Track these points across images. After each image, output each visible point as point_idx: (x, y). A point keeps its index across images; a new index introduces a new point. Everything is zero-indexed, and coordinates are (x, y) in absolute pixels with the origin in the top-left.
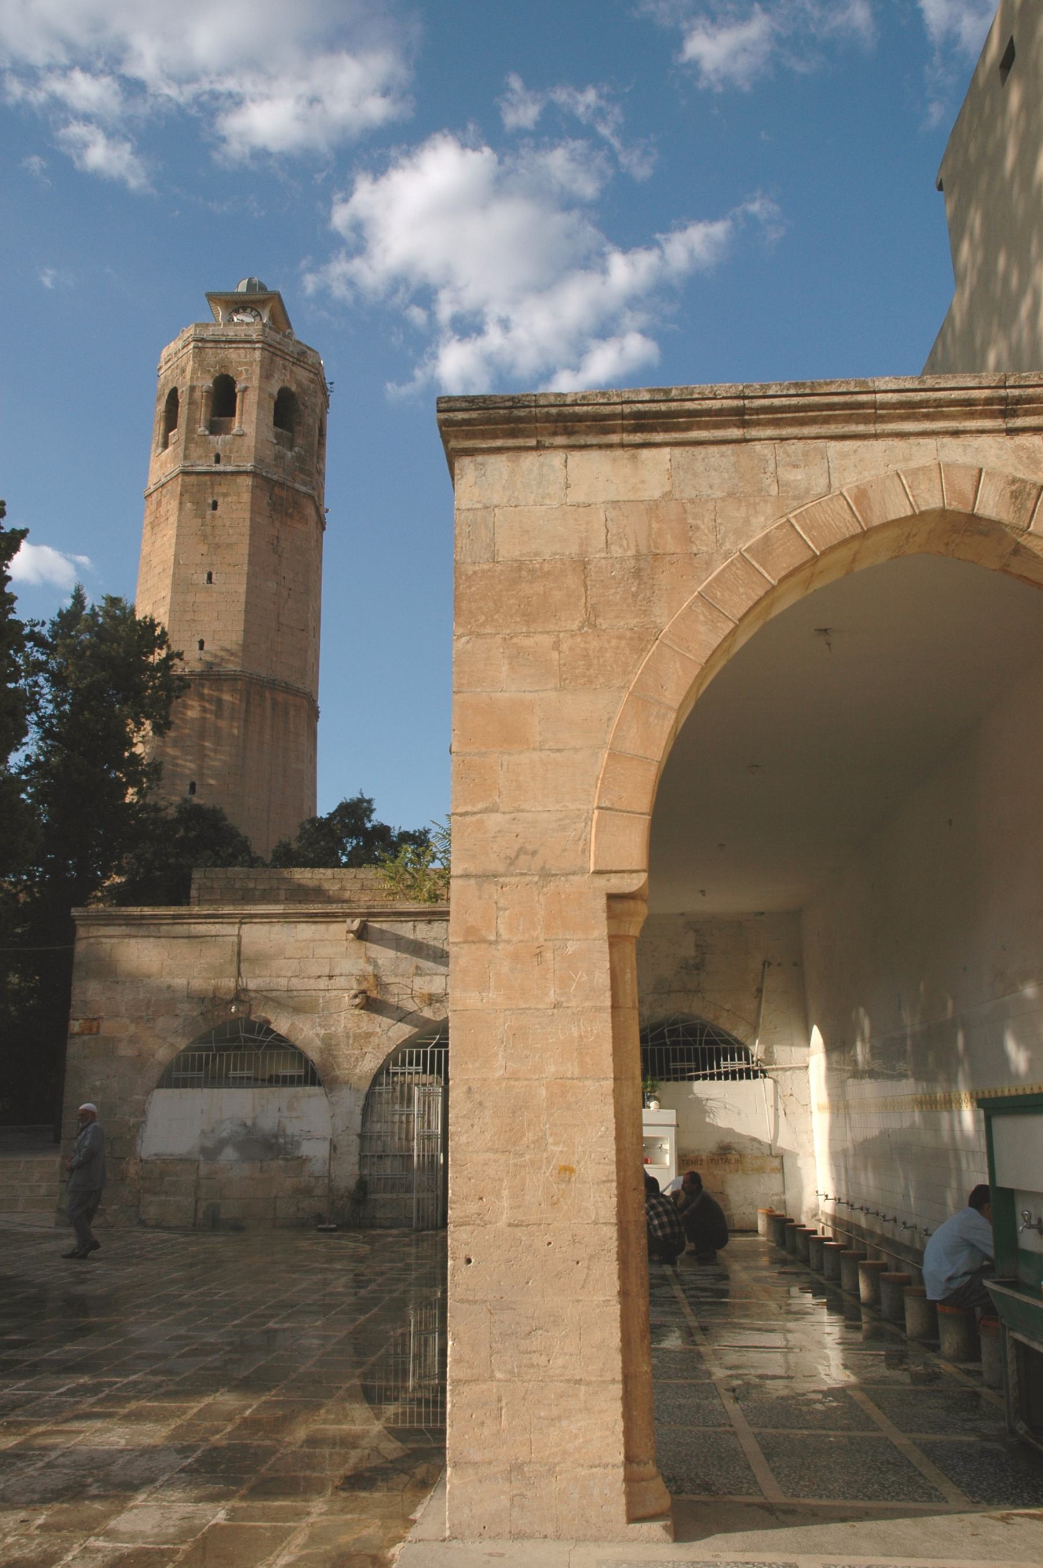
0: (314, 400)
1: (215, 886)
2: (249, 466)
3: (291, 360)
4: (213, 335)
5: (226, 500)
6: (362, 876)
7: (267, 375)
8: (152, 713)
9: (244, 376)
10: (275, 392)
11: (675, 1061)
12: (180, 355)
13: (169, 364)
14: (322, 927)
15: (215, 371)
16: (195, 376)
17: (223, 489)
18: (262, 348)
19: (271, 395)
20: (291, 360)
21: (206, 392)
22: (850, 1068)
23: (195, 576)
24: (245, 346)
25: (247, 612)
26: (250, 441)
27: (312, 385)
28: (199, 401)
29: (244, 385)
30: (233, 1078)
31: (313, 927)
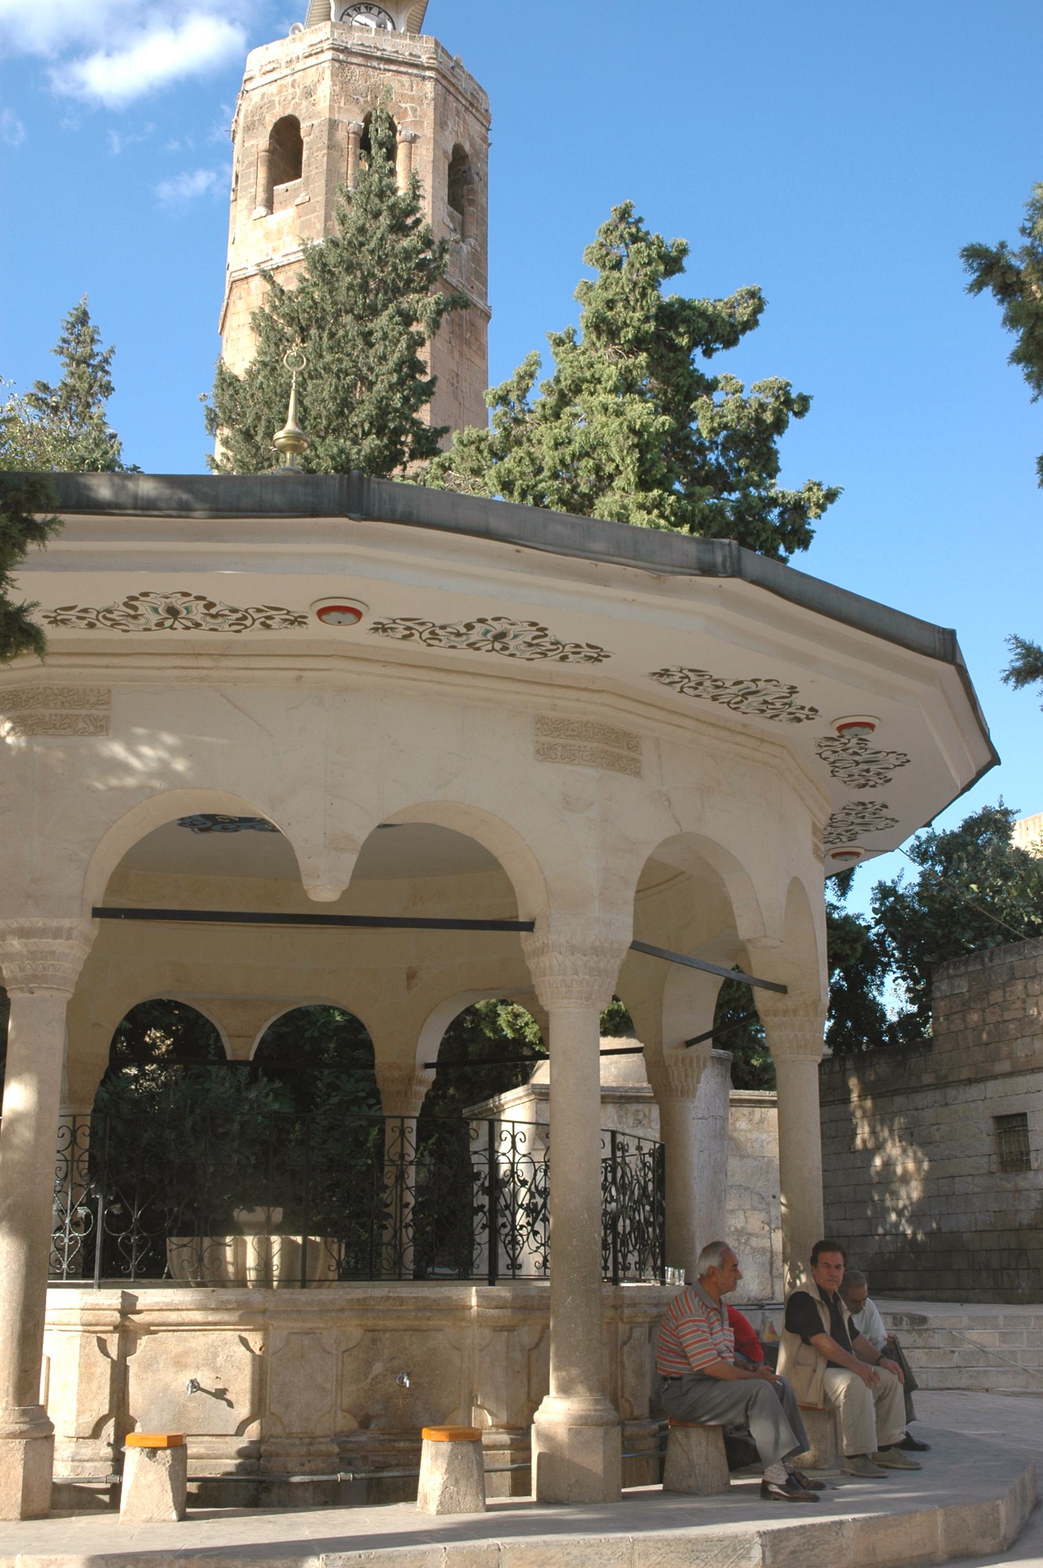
3: (464, 102)
4: (362, 45)
7: (441, 124)
8: (750, 450)
9: (410, 118)
12: (299, 66)
15: (366, 102)
16: (336, 105)
18: (436, 80)
19: (445, 153)
20: (464, 102)
21: (354, 133)
24: (410, 71)
28: (344, 145)
29: (412, 132)
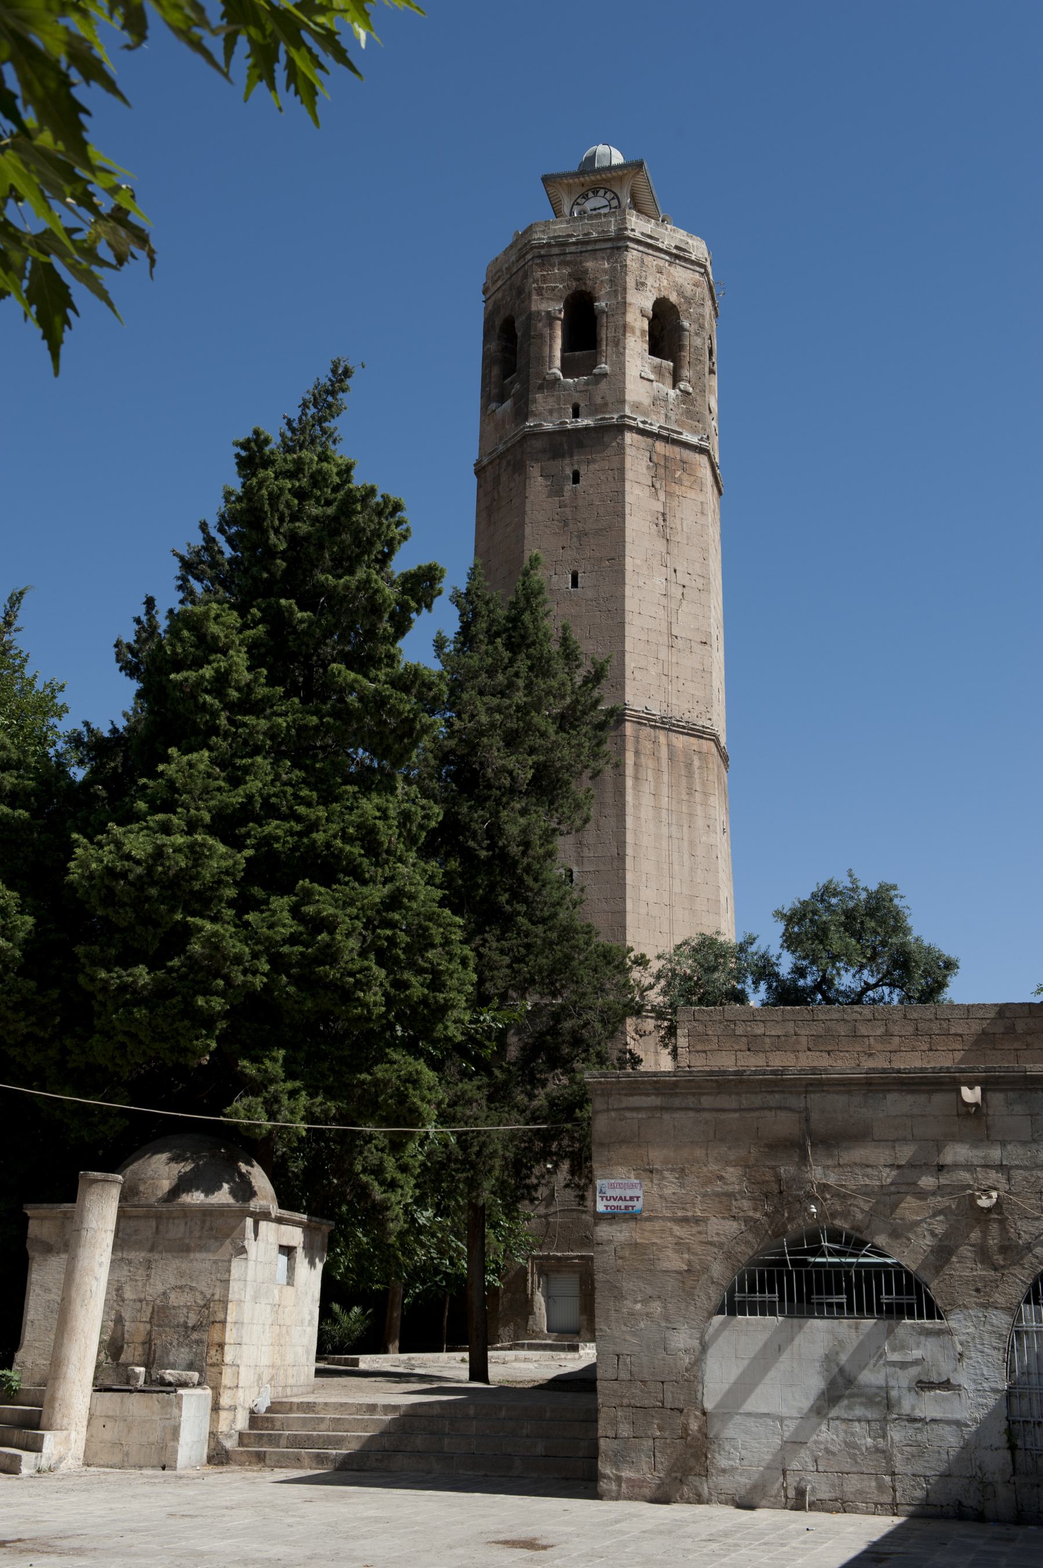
0: (700, 310)
1: (710, 1033)
5: (591, 467)
6: (915, 1015)
10: (648, 305)
11: (820, 1293)
13: (500, 283)
14: (922, 1098)
27: (699, 290)
30: (818, 1304)
31: (910, 1098)
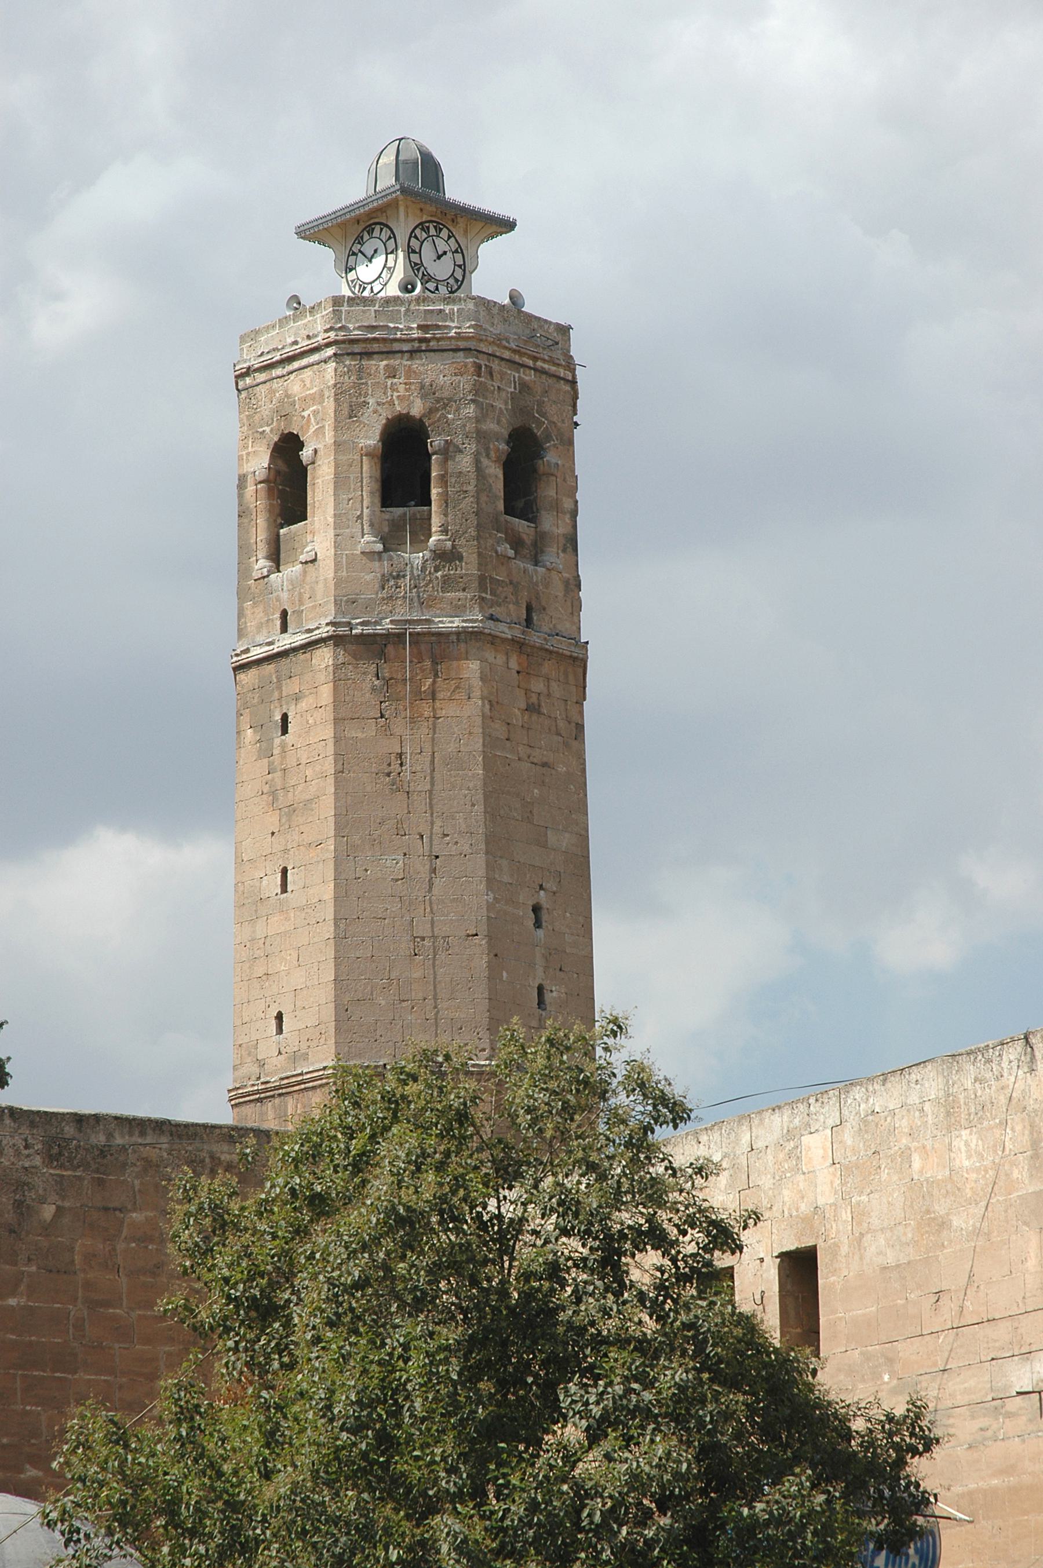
2: (325, 631)
17: (291, 687)
22: (349, 1282)
23: (265, 882)
25: (340, 939)
26: (327, 569)
